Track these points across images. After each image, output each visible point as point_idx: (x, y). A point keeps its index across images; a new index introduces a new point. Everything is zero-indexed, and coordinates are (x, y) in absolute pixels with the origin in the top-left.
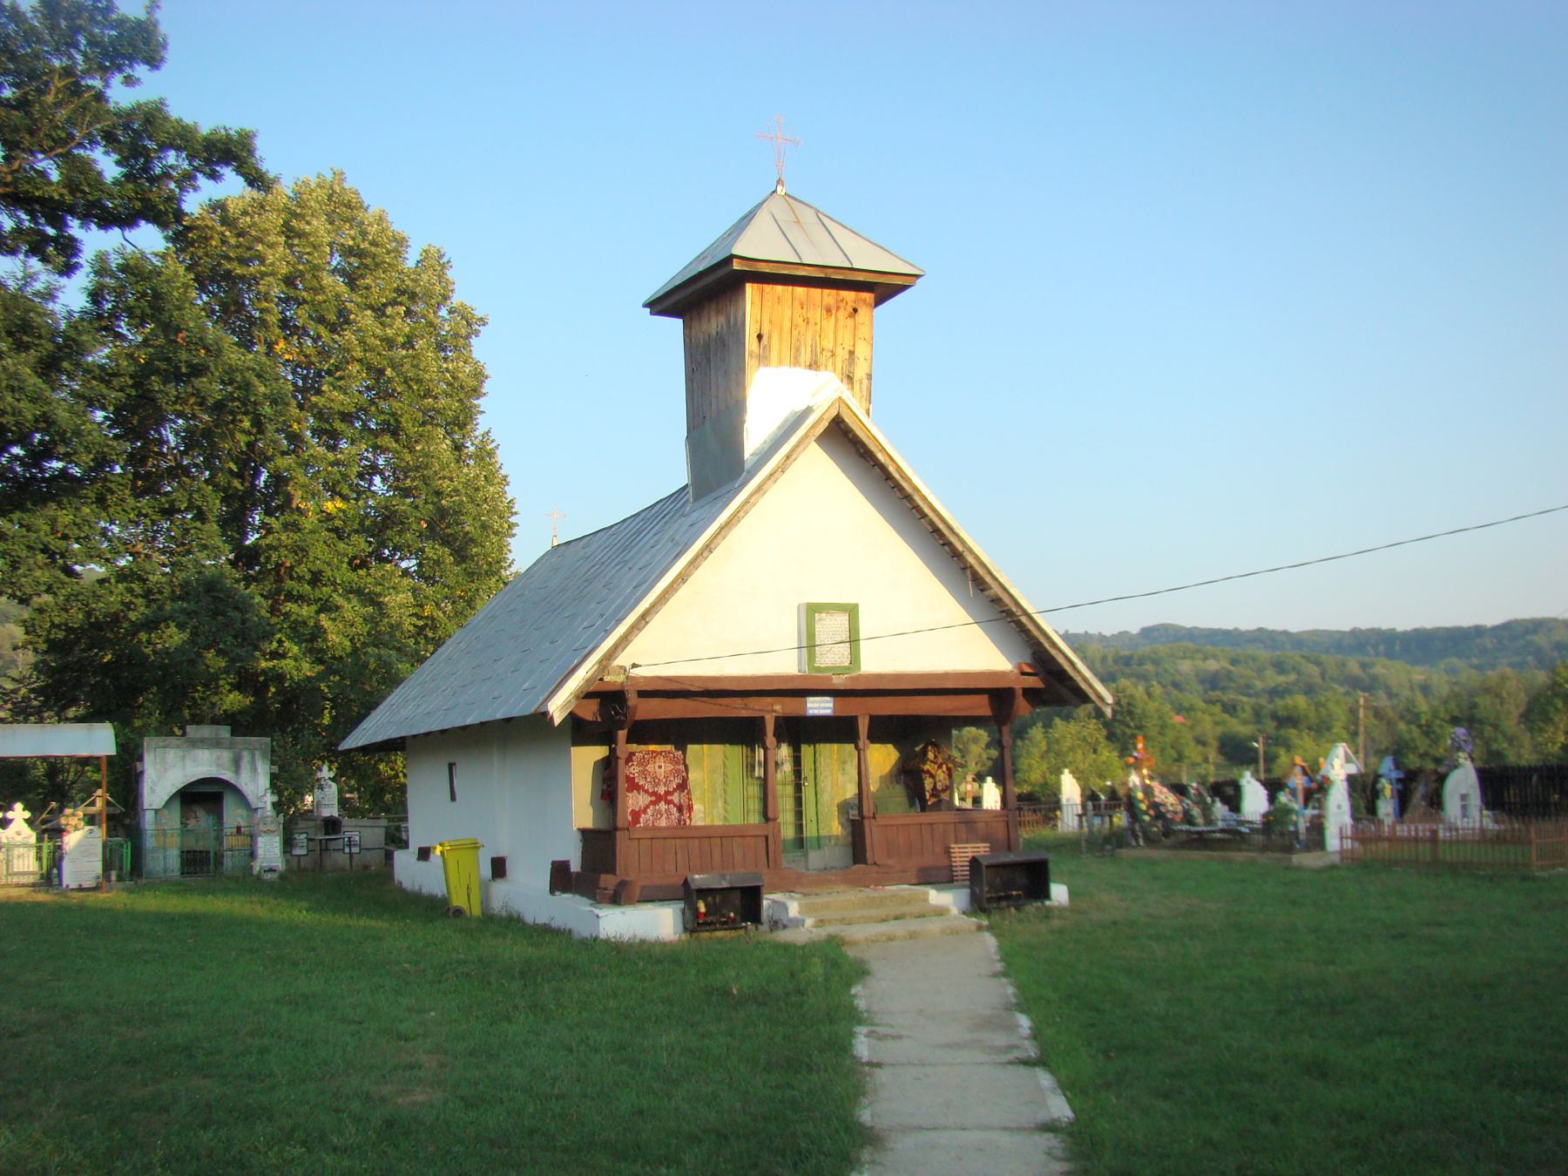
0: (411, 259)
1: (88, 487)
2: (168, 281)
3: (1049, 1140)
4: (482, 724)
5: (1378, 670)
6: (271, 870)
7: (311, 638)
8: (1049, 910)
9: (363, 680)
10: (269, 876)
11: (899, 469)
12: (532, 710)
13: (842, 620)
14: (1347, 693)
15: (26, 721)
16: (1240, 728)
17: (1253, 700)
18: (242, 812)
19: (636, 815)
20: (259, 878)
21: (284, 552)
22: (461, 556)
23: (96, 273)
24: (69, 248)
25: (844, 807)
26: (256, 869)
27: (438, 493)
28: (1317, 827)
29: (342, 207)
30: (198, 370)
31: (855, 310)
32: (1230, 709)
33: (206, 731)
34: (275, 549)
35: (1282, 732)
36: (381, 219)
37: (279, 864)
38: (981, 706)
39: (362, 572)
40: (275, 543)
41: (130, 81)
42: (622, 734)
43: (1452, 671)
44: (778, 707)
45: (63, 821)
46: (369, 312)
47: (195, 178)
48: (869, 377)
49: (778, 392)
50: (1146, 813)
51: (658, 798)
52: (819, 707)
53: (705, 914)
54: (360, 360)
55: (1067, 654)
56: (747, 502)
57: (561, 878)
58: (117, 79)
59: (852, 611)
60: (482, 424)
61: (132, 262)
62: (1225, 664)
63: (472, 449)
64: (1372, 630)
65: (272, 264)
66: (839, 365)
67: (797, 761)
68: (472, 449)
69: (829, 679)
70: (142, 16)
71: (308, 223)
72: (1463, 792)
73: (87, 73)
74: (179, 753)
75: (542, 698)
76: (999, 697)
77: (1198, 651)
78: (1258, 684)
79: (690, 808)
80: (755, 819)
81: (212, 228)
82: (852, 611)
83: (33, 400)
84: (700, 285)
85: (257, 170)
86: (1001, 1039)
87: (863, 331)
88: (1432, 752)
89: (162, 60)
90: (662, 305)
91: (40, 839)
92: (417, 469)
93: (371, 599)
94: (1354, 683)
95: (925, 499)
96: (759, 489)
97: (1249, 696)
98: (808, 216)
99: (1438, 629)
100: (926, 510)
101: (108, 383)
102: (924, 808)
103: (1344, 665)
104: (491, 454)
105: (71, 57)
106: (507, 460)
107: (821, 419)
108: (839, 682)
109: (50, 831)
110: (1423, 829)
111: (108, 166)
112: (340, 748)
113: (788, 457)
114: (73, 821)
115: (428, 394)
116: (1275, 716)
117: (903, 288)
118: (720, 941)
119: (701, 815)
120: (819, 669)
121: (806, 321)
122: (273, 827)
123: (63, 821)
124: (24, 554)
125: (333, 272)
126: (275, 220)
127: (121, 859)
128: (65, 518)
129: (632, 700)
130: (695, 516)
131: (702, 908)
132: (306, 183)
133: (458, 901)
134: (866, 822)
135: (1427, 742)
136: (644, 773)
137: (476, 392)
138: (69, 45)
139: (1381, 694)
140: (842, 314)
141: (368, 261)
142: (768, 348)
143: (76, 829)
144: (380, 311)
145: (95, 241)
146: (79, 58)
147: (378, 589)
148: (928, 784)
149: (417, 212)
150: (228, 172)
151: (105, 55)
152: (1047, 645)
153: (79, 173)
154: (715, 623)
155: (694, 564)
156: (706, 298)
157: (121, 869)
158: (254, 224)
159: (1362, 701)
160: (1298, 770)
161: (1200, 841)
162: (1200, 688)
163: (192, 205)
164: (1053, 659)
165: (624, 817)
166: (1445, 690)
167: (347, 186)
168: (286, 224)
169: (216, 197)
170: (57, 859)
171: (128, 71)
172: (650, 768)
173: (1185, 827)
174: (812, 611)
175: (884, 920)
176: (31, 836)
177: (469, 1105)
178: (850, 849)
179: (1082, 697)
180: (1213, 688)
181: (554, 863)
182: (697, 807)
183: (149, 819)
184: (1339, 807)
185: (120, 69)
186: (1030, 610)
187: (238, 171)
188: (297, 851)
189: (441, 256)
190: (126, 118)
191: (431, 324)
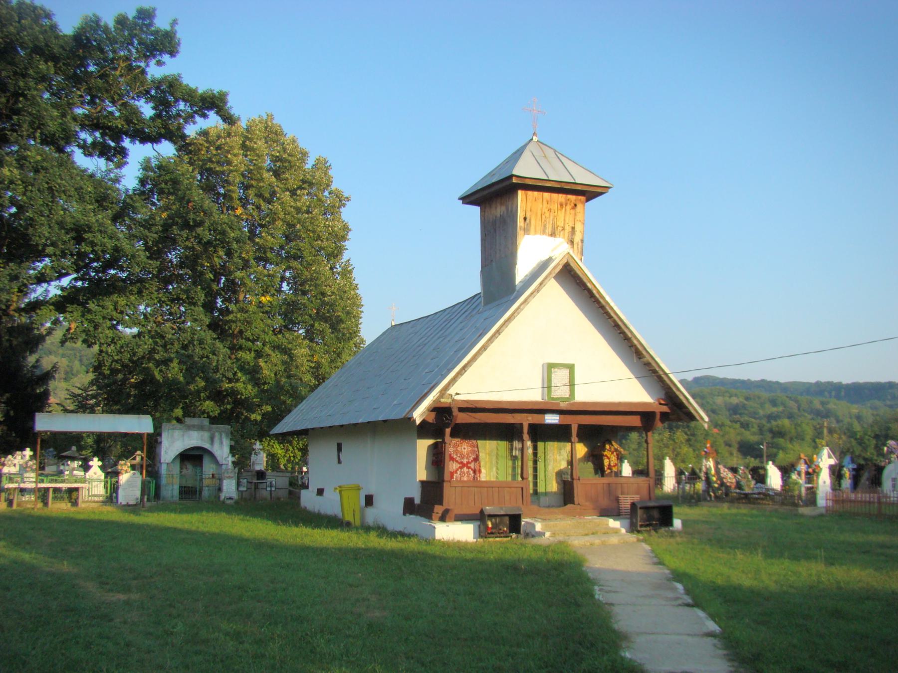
0: (309, 166)
1: (137, 285)
2: (183, 175)
3: (710, 640)
4: (369, 422)
5: (831, 406)
6: (231, 498)
7: (253, 373)
8: (673, 532)
9: (282, 397)
10: (229, 502)
11: (599, 292)
12: (403, 416)
13: (566, 372)
14: (813, 419)
15: (84, 412)
16: (751, 437)
17: (758, 421)
18: (213, 466)
19: (452, 474)
20: (224, 502)
21: (239, 324)
22: (334, 328)
23: (144, 169)
24: (123, 152)
25: (559, 474)
26: (222, 498)
27: (323, 294)
28: (812, 493)
29: (272, 134)
30: (201, 224)
31: (575, 205)
32: (745, 426)
33: (196, 421)
34: (234, 322)
35: (775, 440)
36: (294, 141)
37: (235, 495)
38: (636, 421)
39: (280, 336)
40: (234, 319)
41: (160, 63)
42: (448, 431)
43: (874, 408)
44: (530, 418)
45: (119, 467)
46: (288, 193)
47: (193, 117)
48: (582, 241)
49: (533, 250)
50: (716, 482)
51: (463, 465)
52: (552, 419)
53: (492, 528)
54: (282, 220)
55: (684, 394)
56: (519, 308)
57: (410, 507)
58: (153, 62)
59: (571, 368)
60: (346, 256)
61: (164, 164)
62: (742, 399)
63: (340, 269)
64: (828, 383)
65: (236, 165)
66: (566, 235)
67: (535, 448)
68: (340, 269)
69: (558, 404)
70: (168, 28)
71: (255, 143)
72: (894, 476)
73: (137, 59)
74: (181, 432)
75: (407, 410)
76: (647, 418)
77: (727, 392)
78: (761, 412)
79: (480, 471)
80: (510, 479)
81: (201, 145)
82: (571, 368)
83: (111, 238)
84: (493, 189)
85: (229, 113)
86: (670, 595)
87: (579, 217)
88: (863, 454)
89: (178, 52)
90: (468, 199)
91: (106, 477)
92: (311, 280)
93: (285, 351)
94: (818, 413)
95: (611, 308)
96: (525, 301)
97: (755, 418)
98: (550, 153)
99: (867, 383)
100: (612, 314)
101: (149, 229)
102: (603, 476)
103: (811, 402)
104: (350, 272)
105: (129, 51)
106: (358, 276)
107: (558, 264)
108: (563, 406)
109: (111, 473)
110: (866, 497)
111: (147, 110)
112: (271, 433)
113: (541, 284)
114: (125, 468)
115: (319, 238)
116: (771, 431)
117: (601, 194)
118: (497, 542)
119: (484, 476)
120: (553, 399)
121: (550, 210)
122: (232, 475)
123: (119, 467)
124: (101, 321)
125: (268, 171)
126: (237, 141)
127: (149, 489)
128: (122, 301)
129: (455, 412)
130: (486, 314)
131: (490, 525)
132: (254, 121)
133: (348, 517)
134: (575, 482)
135: (860, 448)
136: (456, 452)
137: (344, 238)
138: (128, 44)
139: (833, 420)
140: (568, 207)
141: (286, 164)
142: (529, 225)
143: (126, 472)
144: (293, 193)
145: (138, 153)
146: (134, 51)
147: (290, 346)
148: (606, 462)
149: (313, 136)
150: (212, 114)
151: (148, 50)
152: (674, 389)
153: (132, 115)
154: (498, 373)
155: (491, 340)
156: (495, 198)
157: (149, 495)
158: (227, 143)
159: (825, 424)
160: (802, 461)
161: (746, 498)
162: (727, 413)
163: (191, 131)
164: (677, 397)
165: (447, 477)
166: (870, 420)
167: (274, 122)
168: (244, 142)
169: (204, 127)
170: (115, 488)
171: (159, 58)
172: (459, 449)
173: (738, 491)
174: (550, 367)
175: (586, 535)
176: (102, 475)
177: (407, 618)
178: (562, 497)
179: (691, 417)
180: (735, 414)
181: (405, 499)
182: (483, 470)
183: (164, 470)
184: (825, 482)
185: (154, 56)
186: (667, 371)
187: (217, 113)
188: (241, 489)
189: (326, 163)
190: (158, 84)
191: (320, 200)
